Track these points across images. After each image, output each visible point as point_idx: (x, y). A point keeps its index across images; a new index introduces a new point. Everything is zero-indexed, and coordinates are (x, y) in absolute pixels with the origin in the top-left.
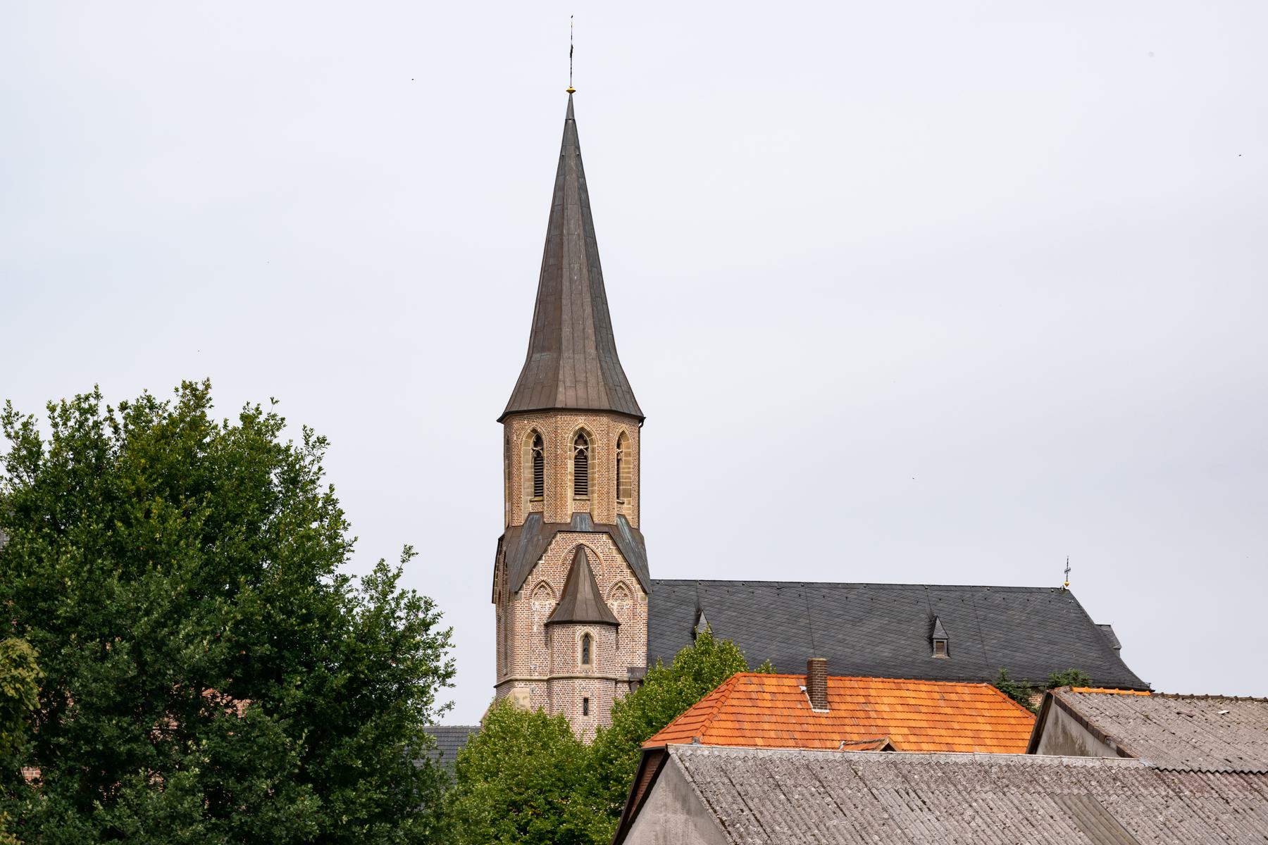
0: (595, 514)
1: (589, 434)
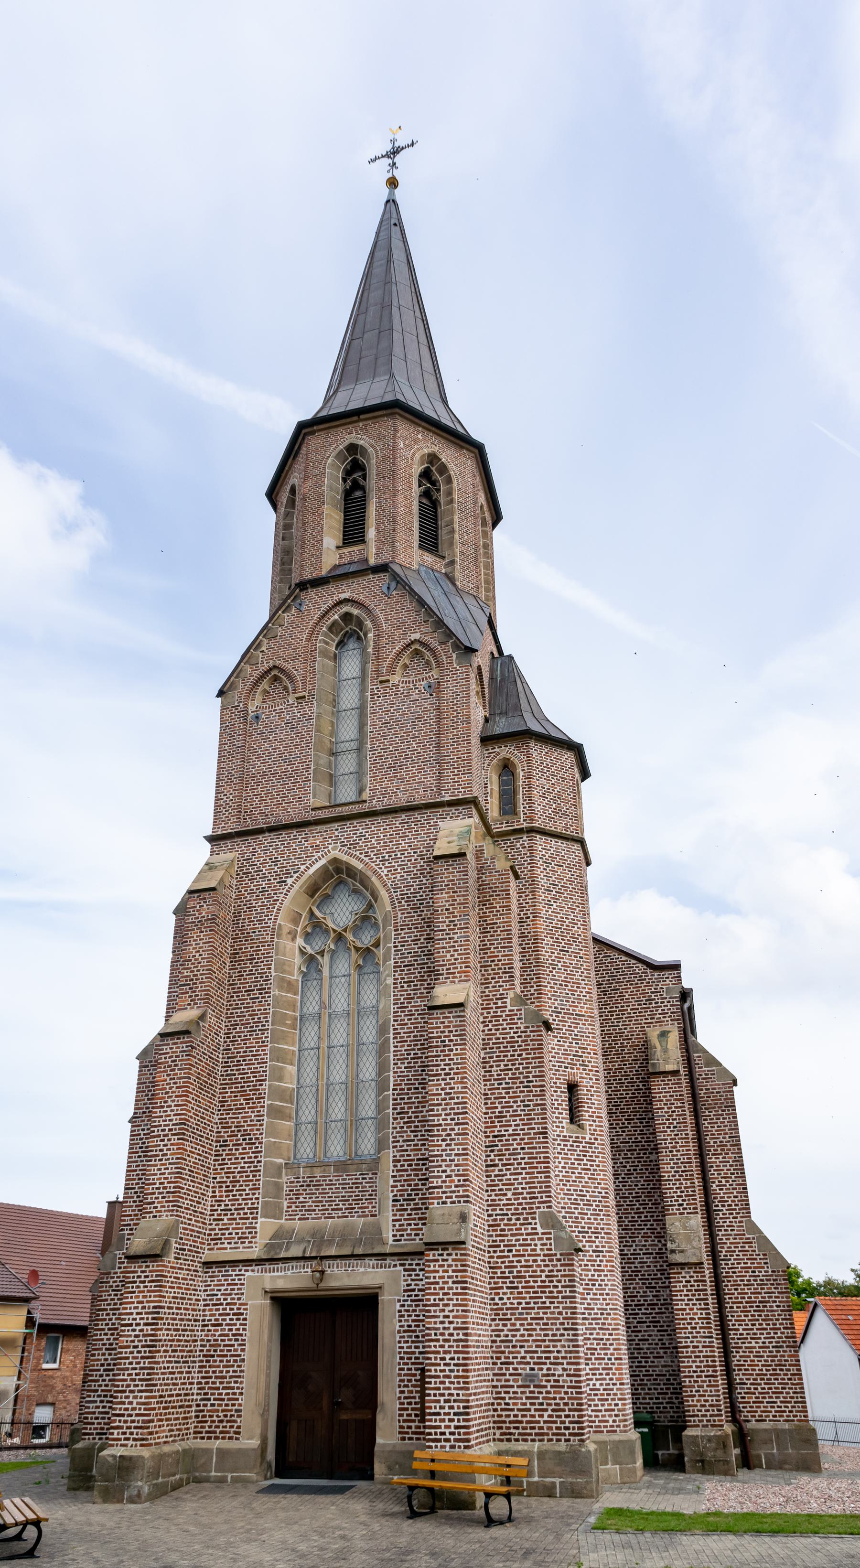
0: (458, 575)
1: (443, 469)
